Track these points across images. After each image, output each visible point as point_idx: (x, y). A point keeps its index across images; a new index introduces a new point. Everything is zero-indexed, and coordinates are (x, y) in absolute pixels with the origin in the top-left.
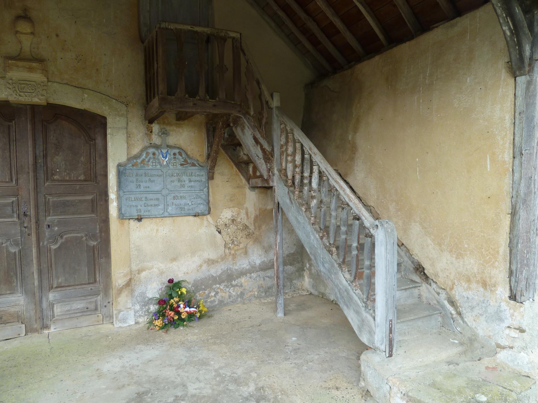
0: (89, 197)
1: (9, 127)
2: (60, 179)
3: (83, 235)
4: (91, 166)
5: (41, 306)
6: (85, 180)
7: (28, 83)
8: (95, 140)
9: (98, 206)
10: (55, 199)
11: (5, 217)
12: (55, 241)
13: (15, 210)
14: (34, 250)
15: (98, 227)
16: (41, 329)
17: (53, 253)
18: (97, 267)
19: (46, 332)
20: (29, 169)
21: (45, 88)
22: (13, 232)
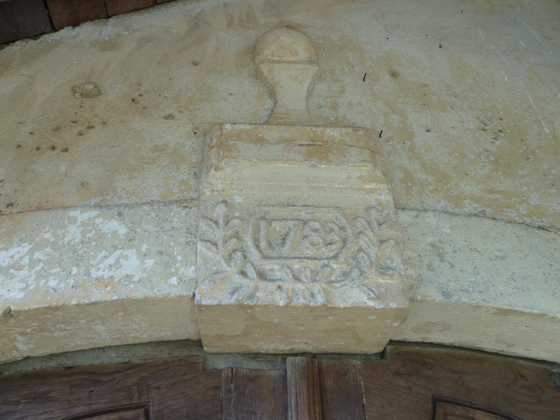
21: (386, 232)
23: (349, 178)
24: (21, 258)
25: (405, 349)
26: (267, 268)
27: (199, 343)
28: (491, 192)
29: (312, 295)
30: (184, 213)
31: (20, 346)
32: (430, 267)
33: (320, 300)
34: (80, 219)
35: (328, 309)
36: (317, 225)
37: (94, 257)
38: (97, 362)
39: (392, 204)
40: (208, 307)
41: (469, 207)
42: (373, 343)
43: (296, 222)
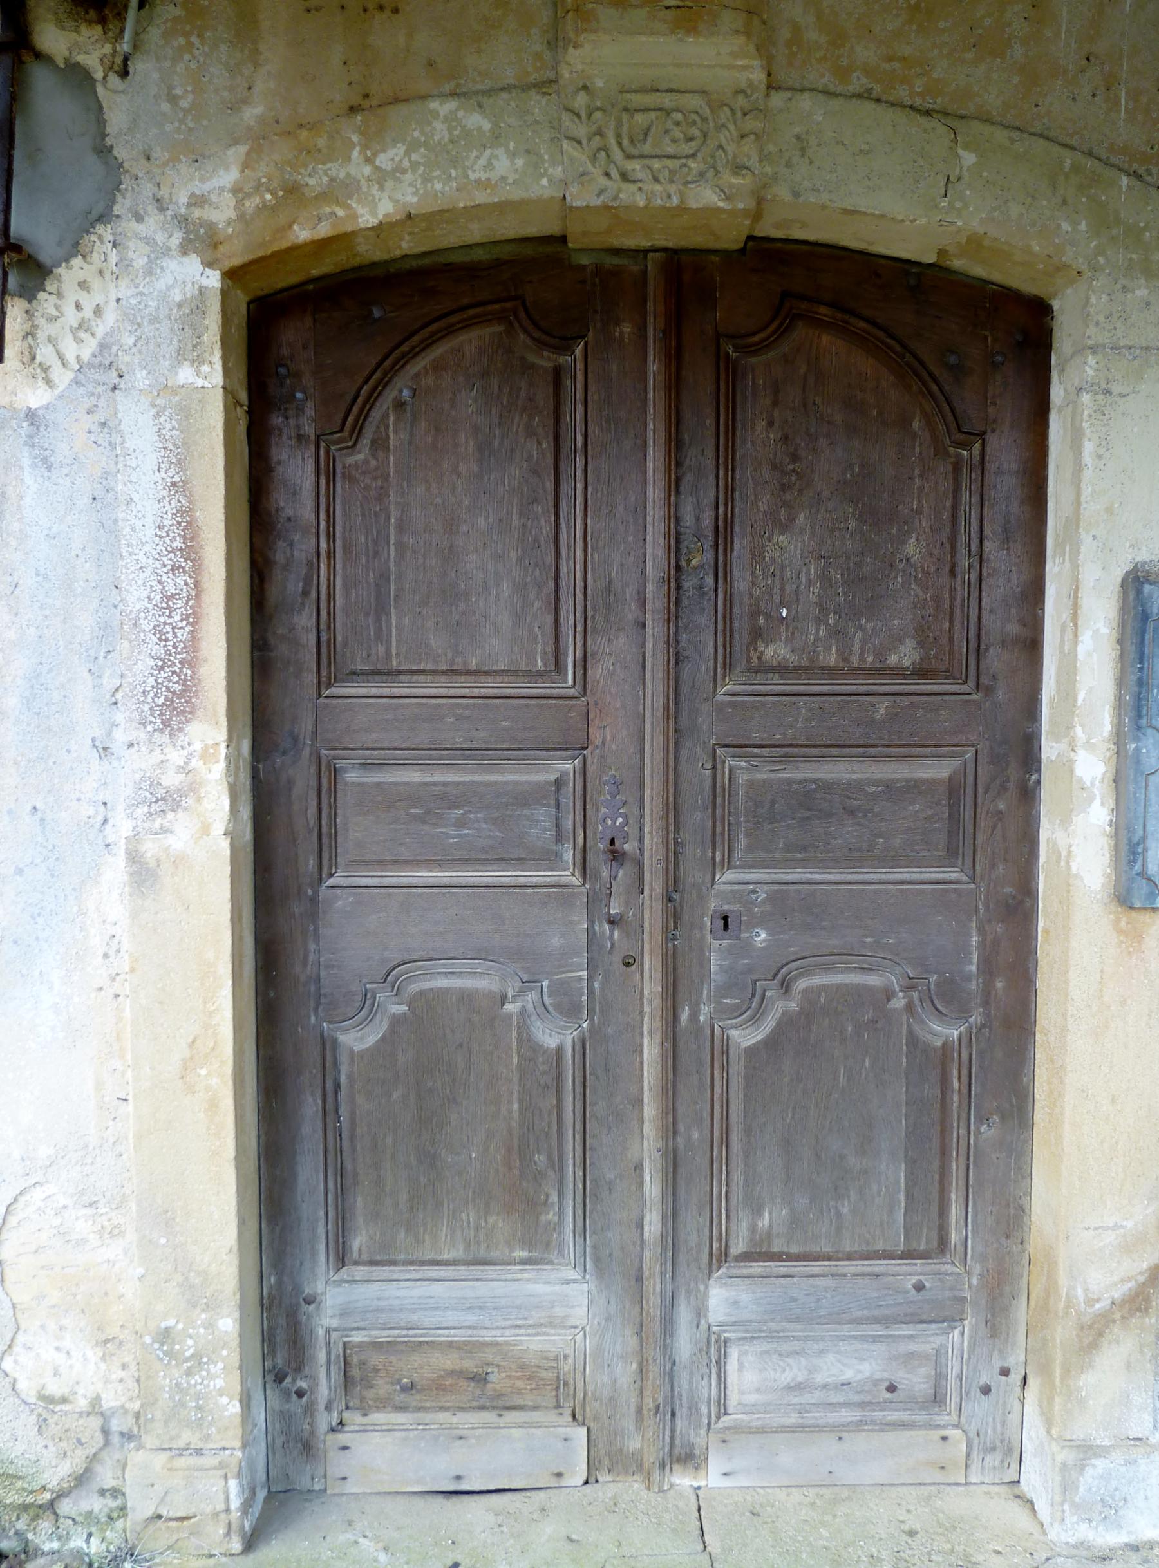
0: (939, 770)
1: (557, 375)
2: (793, 660)
3: (894, 982)
4: (953, 590)
5: (667, 1349)
6: (922, 672)
7: (667, 101)
8: (981, 435)
9: (982, 824)
10: (761, 775)
11: (519, 863)
12: (752, 1007)
13: (568, 824)
14: (651, 1050)
15: (975, 939)
16: (663, 1466)
17: (737, 1068)
18: (955, 1169)
19: (683, 1480)
20: (643, 603)
21: (751, 124)
22: (556, 942)
23: (718, 54)
24: (401, 161)
25: (767, 245)
26: (629, 168)
27: (563, 239)
28: (890, 59)
29: (669, 196)
30: (544, 102)
31: (404, 245)
32: (788, 165)
33: (675, 201)
34: (442, 113)
35: (682, 209)
36: (678, 116)
37: (467, 157)
38: (467, 259)
39: (763, 86)
40: (577, 208)
41: (858, 82)
42: (731, 239)
43: (659, 113)
